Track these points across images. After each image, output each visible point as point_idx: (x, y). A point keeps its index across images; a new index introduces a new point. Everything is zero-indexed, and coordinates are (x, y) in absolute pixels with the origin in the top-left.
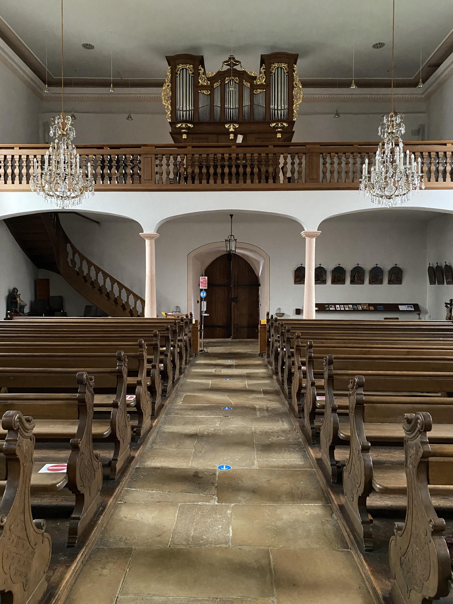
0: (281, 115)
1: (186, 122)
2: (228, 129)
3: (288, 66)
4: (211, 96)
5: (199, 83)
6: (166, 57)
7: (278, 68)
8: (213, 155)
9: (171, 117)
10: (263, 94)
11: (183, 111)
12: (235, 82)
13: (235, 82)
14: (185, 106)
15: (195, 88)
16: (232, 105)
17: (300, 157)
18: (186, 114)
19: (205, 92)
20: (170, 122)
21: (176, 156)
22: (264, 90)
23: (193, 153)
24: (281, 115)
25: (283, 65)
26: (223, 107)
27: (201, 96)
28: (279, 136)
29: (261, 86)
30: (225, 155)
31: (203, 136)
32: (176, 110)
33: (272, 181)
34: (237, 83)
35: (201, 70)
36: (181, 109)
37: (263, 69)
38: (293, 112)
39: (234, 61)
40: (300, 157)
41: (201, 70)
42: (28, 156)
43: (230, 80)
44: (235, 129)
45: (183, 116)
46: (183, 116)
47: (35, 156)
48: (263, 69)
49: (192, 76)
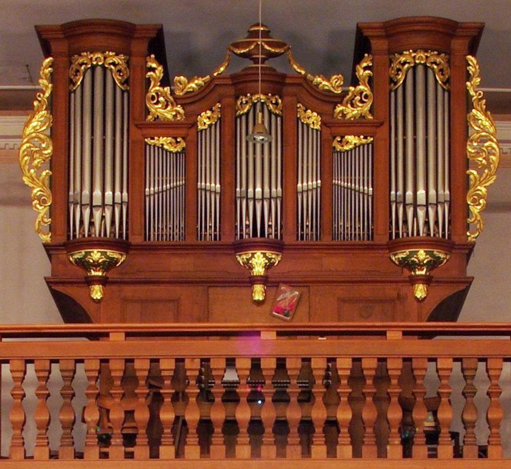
0: (427, 223)
1: (100, 243)
2: (249, 266)
3: (449, 62)
4: (188, 161)
5: (148, 112)
6: (36, 27)
7: (415, 68)
8: (198, 361)
9: (52, 228)
10: (367, 154)
11: (92, 207)
12: (270, 112)
13: (270, 112)
14: (101, 200)
15: (133, 128)
16: (260, 190)
17: (492, 373)
18: (103, 217)
19: (165, 141)
20: (47, 247)
21: (71, 366)
22: (370, 139)
23: (128, 354)
24: (427, 223)
25: (432, 59)
26: (229, 199)
27: (153, 162)
28: (420, 291)
29: (357, 126)
30: (137, 365)
31: (159, 291)
32: (68, 203)
33: (400, 449)
34: (277, 115)
35: (153, 70)
36: (86, 200)
37: (365, 69)
38: (468, 213)
39: (268, 44)
40: (492, 373)
41: (153, 70)
42: (205, 361)
43: (254, 105)
44: (269, 267)
45: (92, 224)
46: (92, 224)
47: (231, 362)
48: (365, 69)
49: (123, 92)
